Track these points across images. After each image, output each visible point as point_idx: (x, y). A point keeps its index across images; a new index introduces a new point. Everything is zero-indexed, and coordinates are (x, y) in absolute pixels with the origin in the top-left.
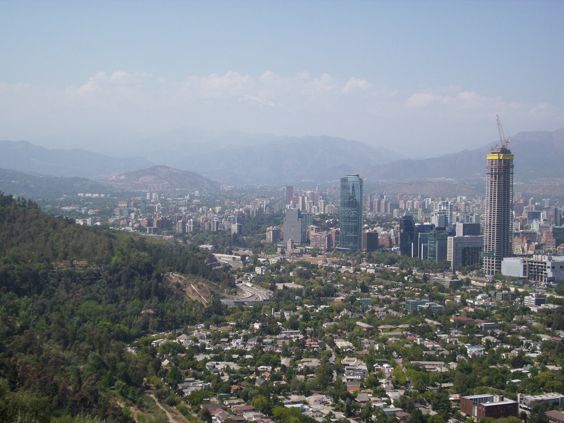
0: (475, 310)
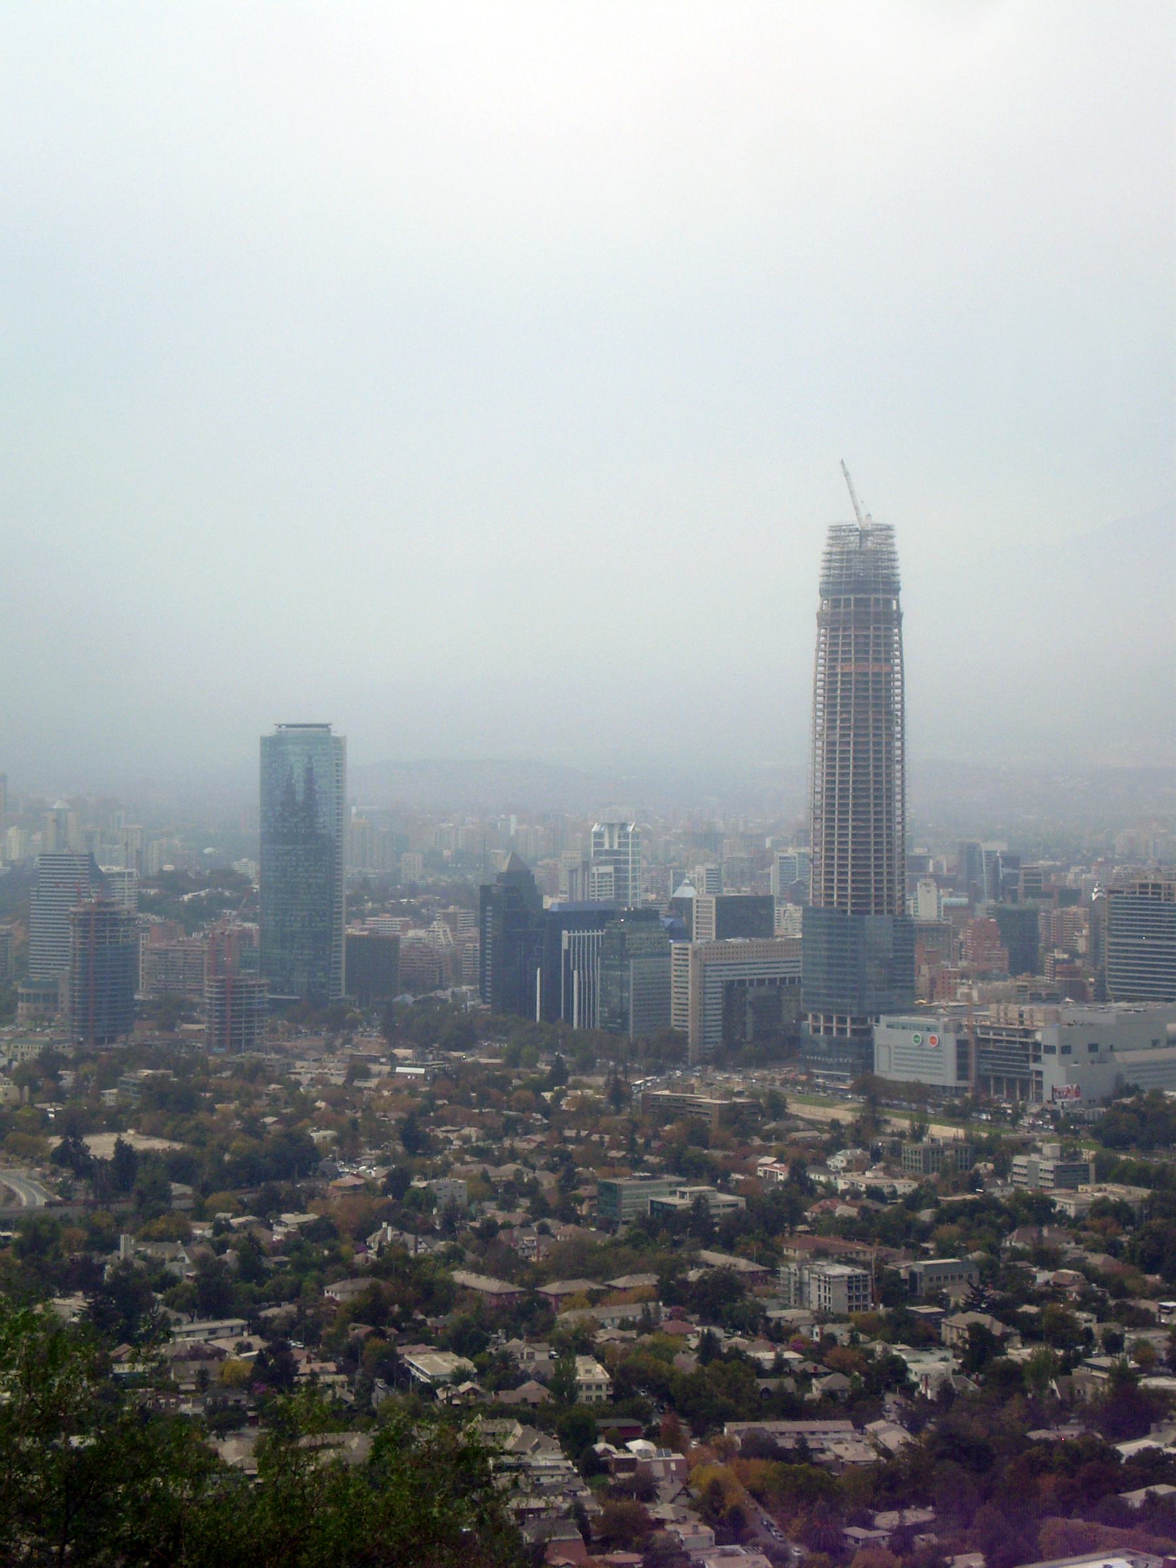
0: (864, 1210)
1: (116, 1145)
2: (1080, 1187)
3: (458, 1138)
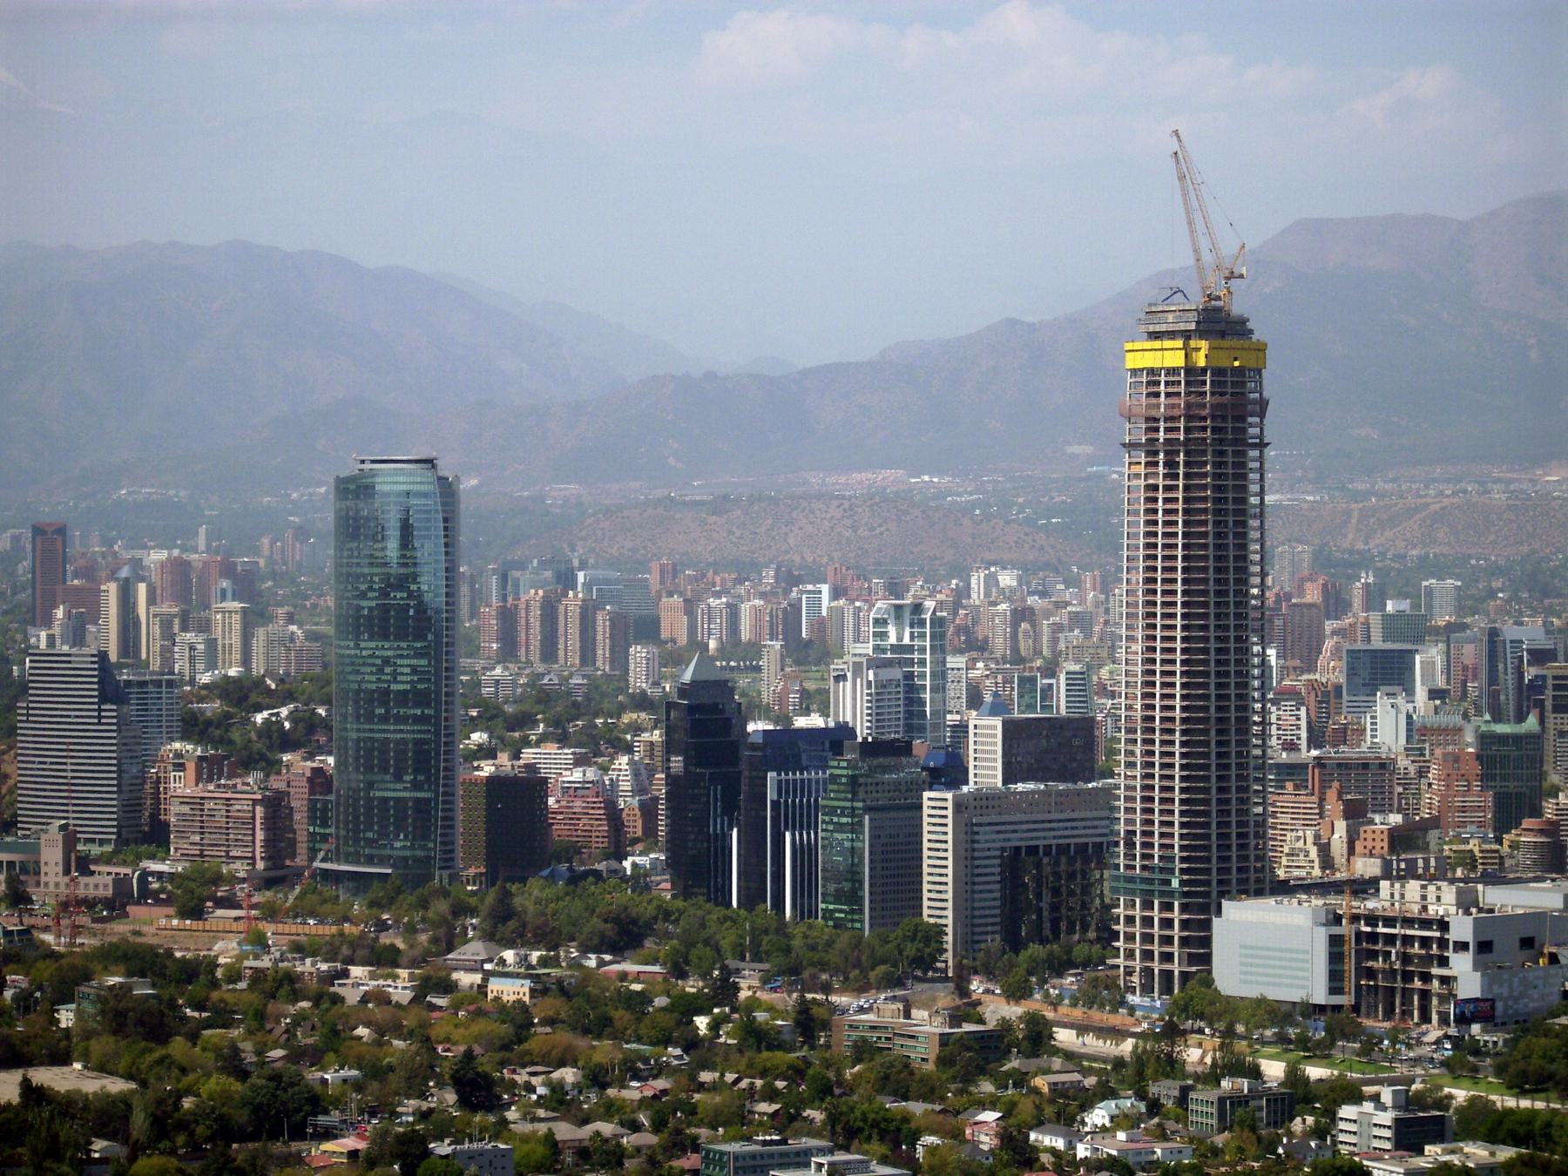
1: (21, 1084)
2: (1427, 1148)
3: (544, 1084)
